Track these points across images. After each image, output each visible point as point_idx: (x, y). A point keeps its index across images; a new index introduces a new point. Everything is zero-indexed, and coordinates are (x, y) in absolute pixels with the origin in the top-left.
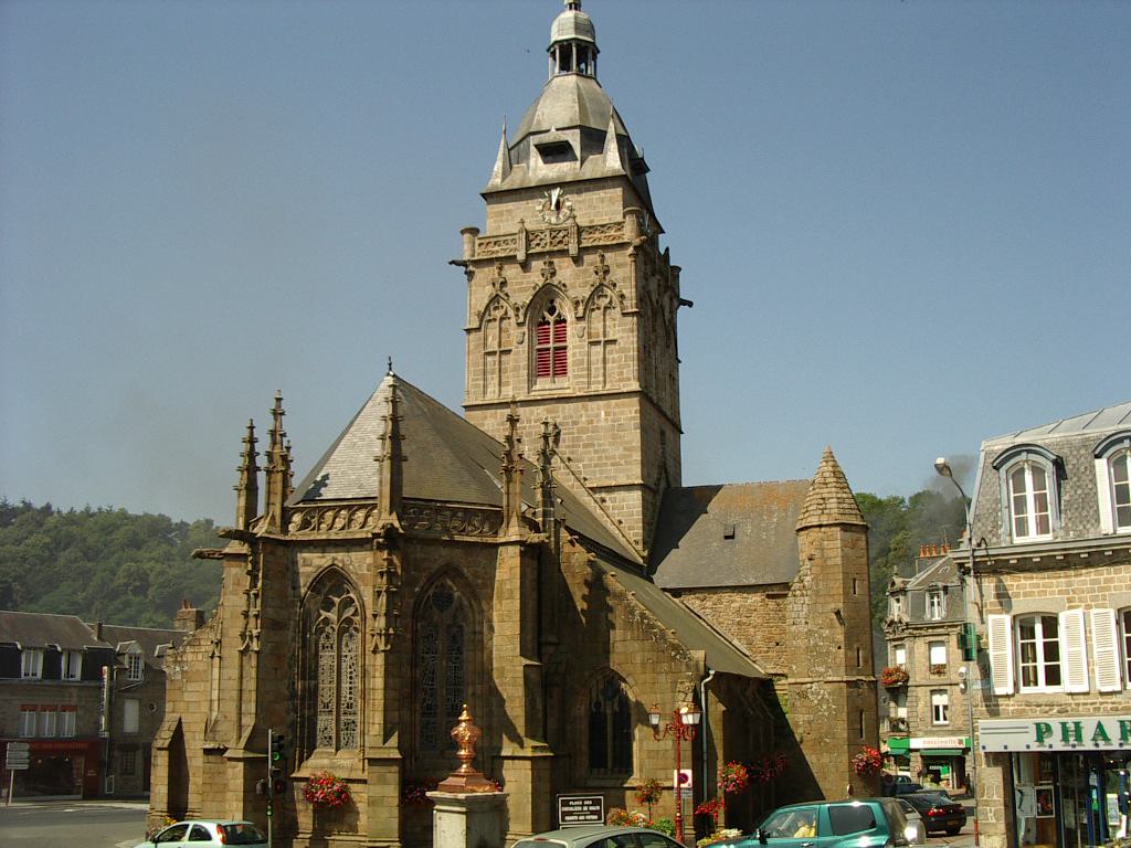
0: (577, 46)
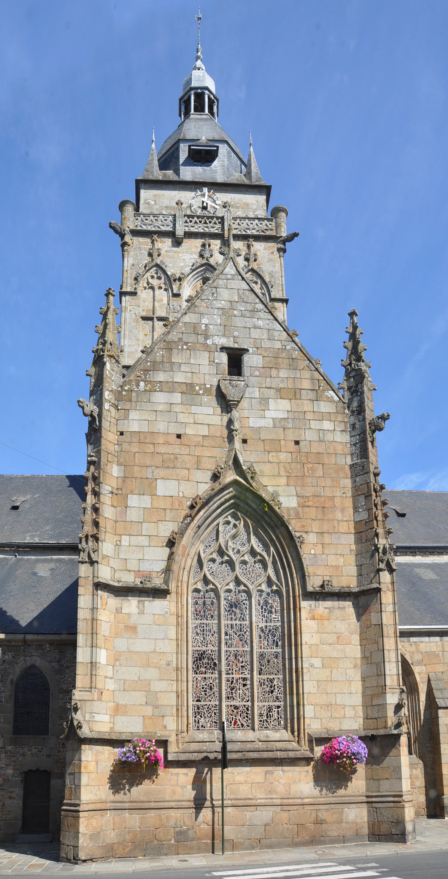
0: (196, 94)
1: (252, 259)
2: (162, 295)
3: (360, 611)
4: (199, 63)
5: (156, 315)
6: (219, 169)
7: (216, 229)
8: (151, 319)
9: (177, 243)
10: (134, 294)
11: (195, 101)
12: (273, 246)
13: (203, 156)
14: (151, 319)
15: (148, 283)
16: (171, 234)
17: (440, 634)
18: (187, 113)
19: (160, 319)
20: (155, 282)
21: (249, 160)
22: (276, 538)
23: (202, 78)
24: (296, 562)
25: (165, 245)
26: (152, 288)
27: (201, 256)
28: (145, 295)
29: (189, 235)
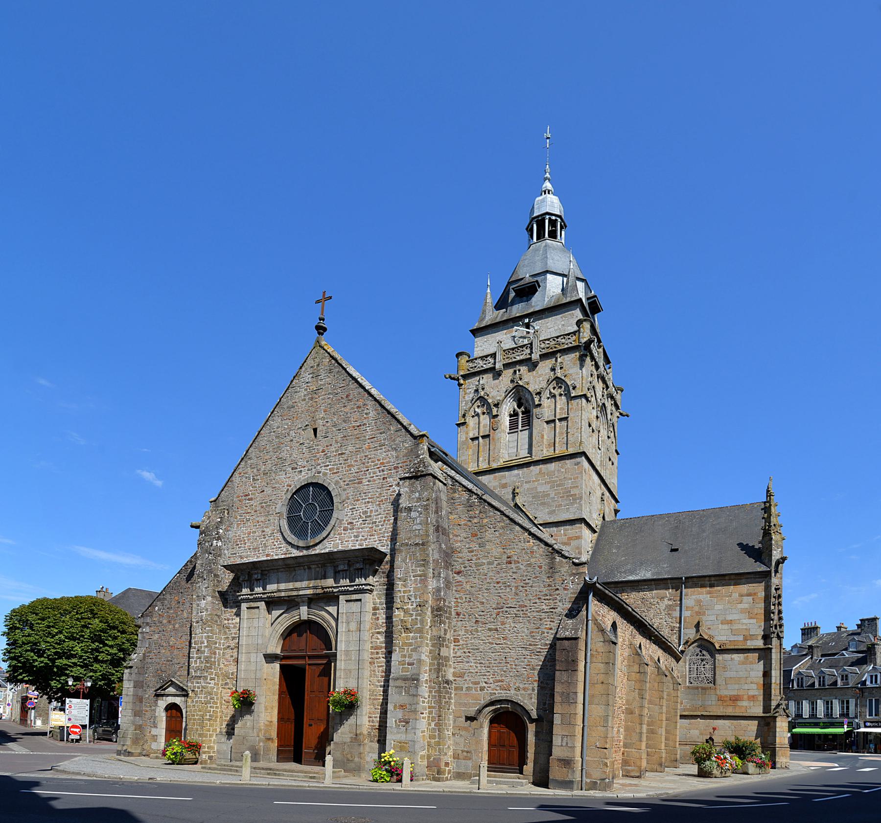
2: (485, 420)
20: (479, 411)
23: (551, 204)
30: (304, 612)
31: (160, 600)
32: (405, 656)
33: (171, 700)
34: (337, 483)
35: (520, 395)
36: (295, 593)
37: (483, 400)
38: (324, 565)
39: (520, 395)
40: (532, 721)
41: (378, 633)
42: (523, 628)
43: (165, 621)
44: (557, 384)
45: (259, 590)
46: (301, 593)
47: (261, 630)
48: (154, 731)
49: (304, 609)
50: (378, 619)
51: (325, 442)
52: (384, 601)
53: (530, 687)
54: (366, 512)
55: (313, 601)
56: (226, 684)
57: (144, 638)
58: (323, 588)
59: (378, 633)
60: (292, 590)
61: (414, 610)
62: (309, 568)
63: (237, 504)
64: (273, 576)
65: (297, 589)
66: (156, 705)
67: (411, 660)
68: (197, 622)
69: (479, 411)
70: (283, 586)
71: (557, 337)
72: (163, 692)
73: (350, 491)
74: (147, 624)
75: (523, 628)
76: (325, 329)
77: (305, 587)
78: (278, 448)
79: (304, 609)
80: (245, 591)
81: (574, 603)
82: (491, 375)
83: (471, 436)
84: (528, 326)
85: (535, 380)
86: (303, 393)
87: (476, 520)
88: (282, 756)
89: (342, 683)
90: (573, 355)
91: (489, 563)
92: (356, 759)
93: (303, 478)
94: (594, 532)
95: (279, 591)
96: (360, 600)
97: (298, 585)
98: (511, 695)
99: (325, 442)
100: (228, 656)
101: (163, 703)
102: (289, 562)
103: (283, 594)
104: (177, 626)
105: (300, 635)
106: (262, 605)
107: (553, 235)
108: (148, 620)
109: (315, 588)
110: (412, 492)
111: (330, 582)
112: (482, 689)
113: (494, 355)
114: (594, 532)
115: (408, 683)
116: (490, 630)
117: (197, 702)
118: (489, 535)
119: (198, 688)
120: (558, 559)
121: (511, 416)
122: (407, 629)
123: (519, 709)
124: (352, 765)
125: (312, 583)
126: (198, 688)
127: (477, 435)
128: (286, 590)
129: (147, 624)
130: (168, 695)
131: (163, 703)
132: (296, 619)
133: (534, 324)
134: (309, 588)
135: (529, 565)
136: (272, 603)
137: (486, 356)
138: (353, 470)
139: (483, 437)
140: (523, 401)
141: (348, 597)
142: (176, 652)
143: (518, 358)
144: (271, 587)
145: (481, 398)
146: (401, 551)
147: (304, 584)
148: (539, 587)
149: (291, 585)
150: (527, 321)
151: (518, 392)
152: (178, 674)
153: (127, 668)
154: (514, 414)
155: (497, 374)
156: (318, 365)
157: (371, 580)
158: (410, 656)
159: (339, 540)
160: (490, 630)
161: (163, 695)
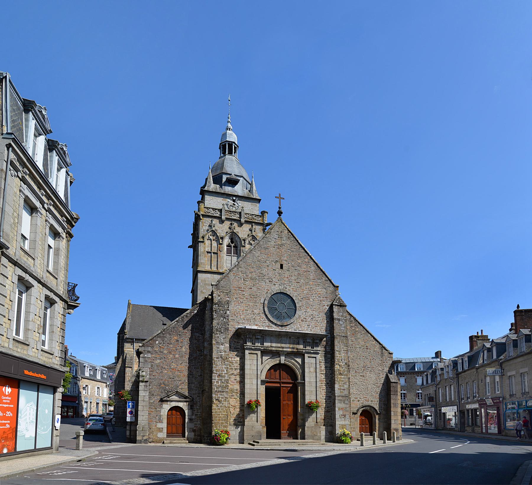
1: (253, 231)
2: (215, 244)
3: (26, 102)
4: (229, 125)
5: (213, 251)
6: (239, 189)
7: (236, 217)
8: (210, 253)
9: (222, 222)
10: (203, 242)
11: (227, 148)
12: (261, 227)
13: (233, 182)
14: (210, 253)
15: (209, 237)
16: (219, 218)
17: (330, 395)
18: (224, 153)
19: (214, 253)
20: (211, 237)
21: (252, 182)
22: (298, 391)
23: (232, 137)
24: (302, 400)
25: (216, 221)
26: (210, 240)
27: (230, 228)
28: (207, 242)
29: (227, 219)
30: (283, 359)
31: (160, 337)
32: (340, 386)
33: (174, 404)
34: (296, 296)
35: (233, 237)
36: (281, 349)
37: (214, 233)
38: (298, 338)
39: (233, 237)
40: (377, 414)
41: (322, 374)
42: (373, 376)
43: (165, 352)
44: (253, 238)
45: (258, 344)
46: (285, 350)
47: (257, 367)
48: (159, 425)
49: (283, 358)
50: (321, 367)
51: (287, 274)
52: (323, 359)
53: (376, 400)
54: (312, 315)
55: (288, 354)
56: (232, 396)
57: (146, 361)
58: (297, 349)
59: (322, 374)
60: (279, 347)
61: (344, 365)
62: (290, 338)
63: (233, 291)
64: (268, 338)
65: (283, 348)
66: (161, 407)
67: (344, 388)
68: (217, 358)
69: (211, 237)
70: (274, 345)
71: (253, 215)
72: (168, 399)
73: (304, 302)
74: (149, 352)
75: (373, 376)
76: (282, 213)
77: (287, 347)
78: (259, 267)
79: (283, 358)
80: (249, 344)
81: (389, 368)
82: (218, 221)
83: (207, 250)
84: (234, 201)
85: (243, 232)
86: (273, 243)
87: (353, 328)
88: (268, 437)
89: (309, 398)
90: (260, 227)
91: (360, 348)
92: (319, 434)
93: (276, 289)
94: (2, 264)
95: (271, 347)
96: (315, 358)
97: (283, 345)
98: (369, 403)
99: (287, 274)
100: (232, 379)
101: (166, 407)
102: (282, 333)
103: (274, 349)
104: (177, 356)
105: (275, 371)
106: (259, 353)
107: (230, 153)
108: (149, 349)
109: (293, 348)
110: (339, 312)
111: (301, 347)
112: (359, 401)
113: (221, 211)
114: (2, 264)
115: (344, 398)
116: (361, 376)
117: (221, 406)
118: (359, 335)
119: (222, 398)
120: (384, 350)
121: (227, 246)
122: (341, 374)
123: (372, 409)
124: (317, 437)
125: (291, 346)
126: (222, 398)
127: (210, 251)
128: (275, 347)
129: (149, 352)
130: (172, 401)
131: (166, 407)
132: (278, 362)
133: (238, 202)
134: (290, 348)
135: (374, 351)
136: (264, 352)
137: (216, 209)
138: (305, 292)
139: (214, 253)
140: (235, 241)
141: (310, 355)
142: (177, 373)
143: (233, 218)
144: (266, 344)
145: (213, 231)
146: (337, 338)
147: (288, 345)
148: (378, 361)
149: (279, 345)
150: (234, 198)
151: (232, 235)
152: (180, 387)
153: (142, 382)
154: (229, 246)
155: (222, 222)
156: (281, 232)
157: (318, 349)
158: (343, 386)
159: (297, 326)
160: (361, 376)
161: (167, 401)
